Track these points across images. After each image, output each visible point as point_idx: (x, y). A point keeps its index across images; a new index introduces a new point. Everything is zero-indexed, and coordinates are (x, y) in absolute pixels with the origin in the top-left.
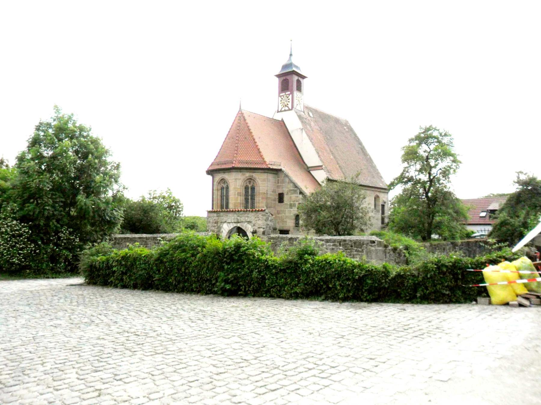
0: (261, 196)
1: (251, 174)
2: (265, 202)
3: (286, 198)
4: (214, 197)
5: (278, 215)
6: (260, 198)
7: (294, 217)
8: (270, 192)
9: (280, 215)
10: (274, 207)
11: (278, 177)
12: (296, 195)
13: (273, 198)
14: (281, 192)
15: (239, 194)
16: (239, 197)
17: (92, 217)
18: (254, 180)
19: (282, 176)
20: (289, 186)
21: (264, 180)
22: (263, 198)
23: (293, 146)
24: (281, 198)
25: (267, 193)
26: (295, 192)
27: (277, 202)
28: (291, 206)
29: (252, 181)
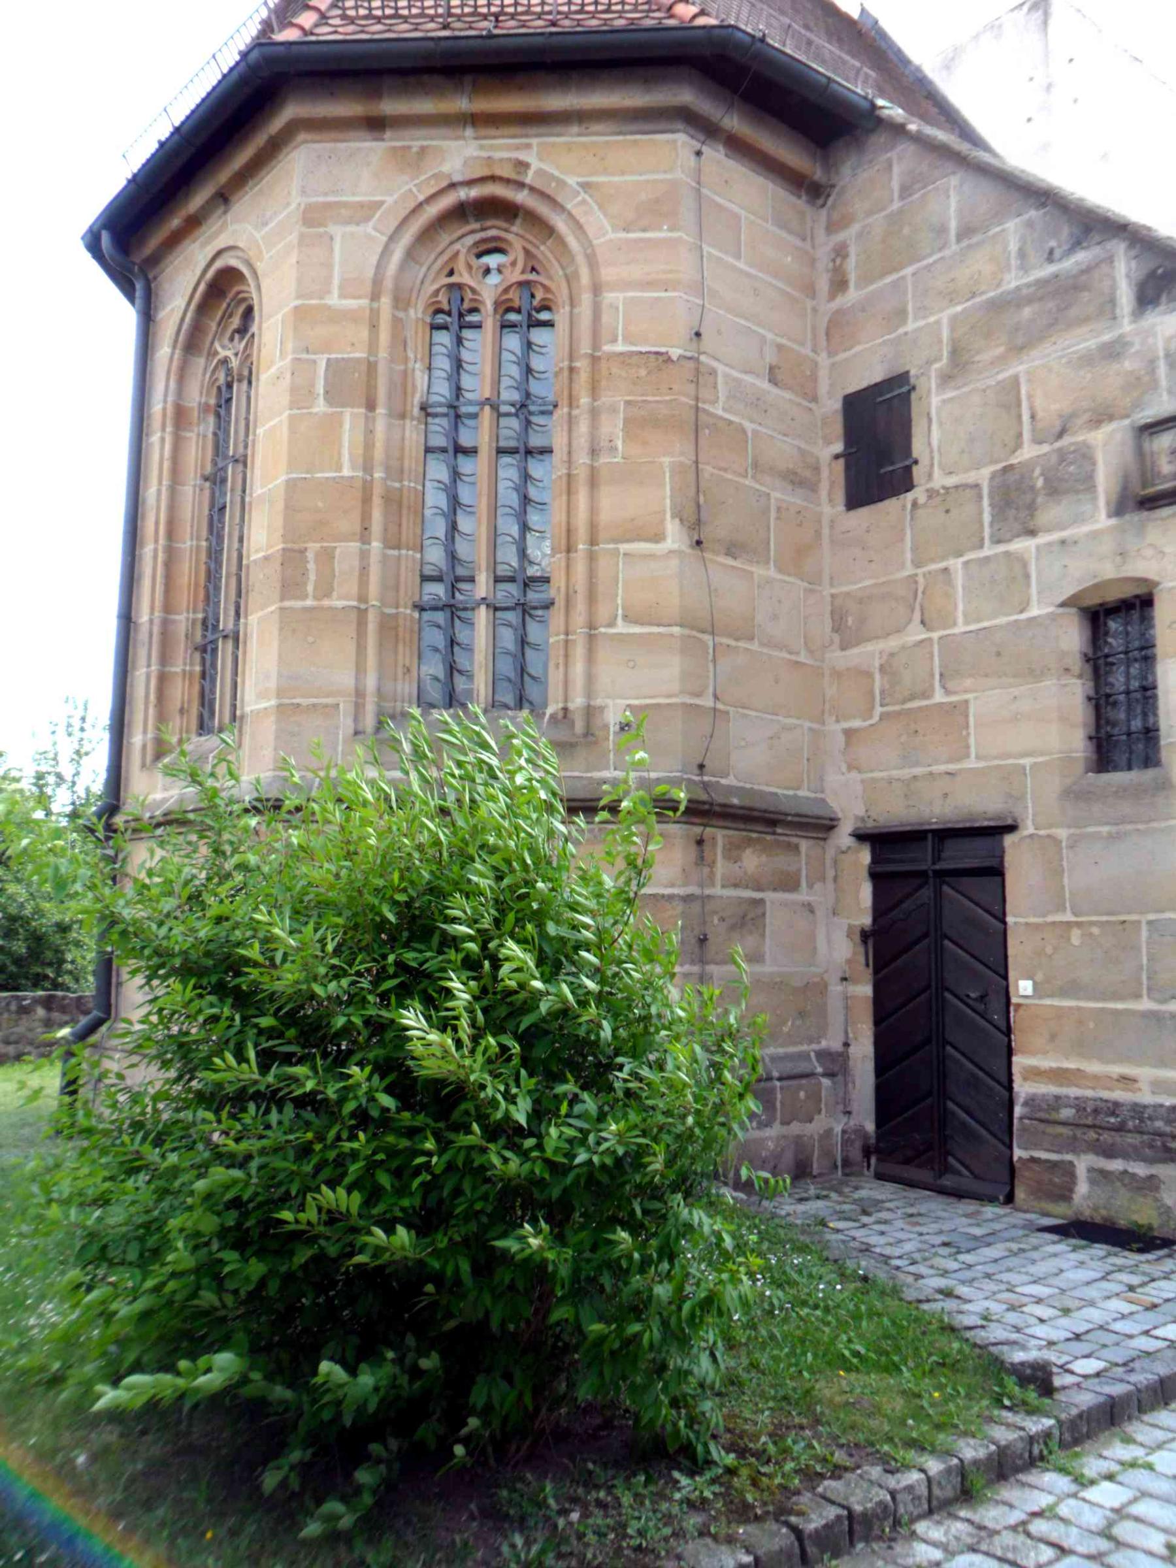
0: (615, 397)
1: (501, 149)
2: (670, 456)
3: (942, 435)
4: (153, 492)
5: (839, 658)
6: (613, 428)
7: (1072, 638)
8: (734, 365)
9: (869, 653)
10: (798, 558)
11: (832, 227)
12: (1086, 340)
13: (783, 449)
14: (867, 371)
15: (355, 385)
16: (350, 419)
17: (738, 1458)
18: (534, 220)
19: (875, 182)
20: (979, 264)
21: (657, 209)
22: (639, 424)
23: (961, 942)
24: (875, 448)
25: (700, 374)
26: (1063, 299)
27: (841, 508)
28: (1017, 501)
29: (515, 235)
